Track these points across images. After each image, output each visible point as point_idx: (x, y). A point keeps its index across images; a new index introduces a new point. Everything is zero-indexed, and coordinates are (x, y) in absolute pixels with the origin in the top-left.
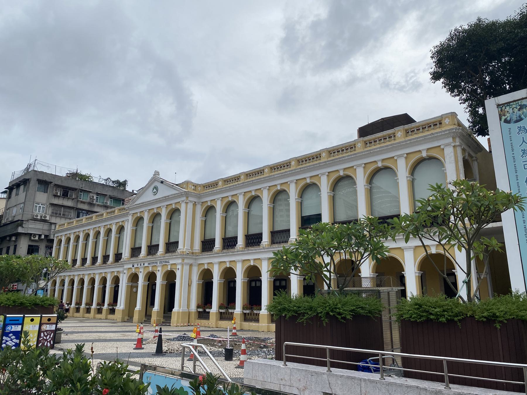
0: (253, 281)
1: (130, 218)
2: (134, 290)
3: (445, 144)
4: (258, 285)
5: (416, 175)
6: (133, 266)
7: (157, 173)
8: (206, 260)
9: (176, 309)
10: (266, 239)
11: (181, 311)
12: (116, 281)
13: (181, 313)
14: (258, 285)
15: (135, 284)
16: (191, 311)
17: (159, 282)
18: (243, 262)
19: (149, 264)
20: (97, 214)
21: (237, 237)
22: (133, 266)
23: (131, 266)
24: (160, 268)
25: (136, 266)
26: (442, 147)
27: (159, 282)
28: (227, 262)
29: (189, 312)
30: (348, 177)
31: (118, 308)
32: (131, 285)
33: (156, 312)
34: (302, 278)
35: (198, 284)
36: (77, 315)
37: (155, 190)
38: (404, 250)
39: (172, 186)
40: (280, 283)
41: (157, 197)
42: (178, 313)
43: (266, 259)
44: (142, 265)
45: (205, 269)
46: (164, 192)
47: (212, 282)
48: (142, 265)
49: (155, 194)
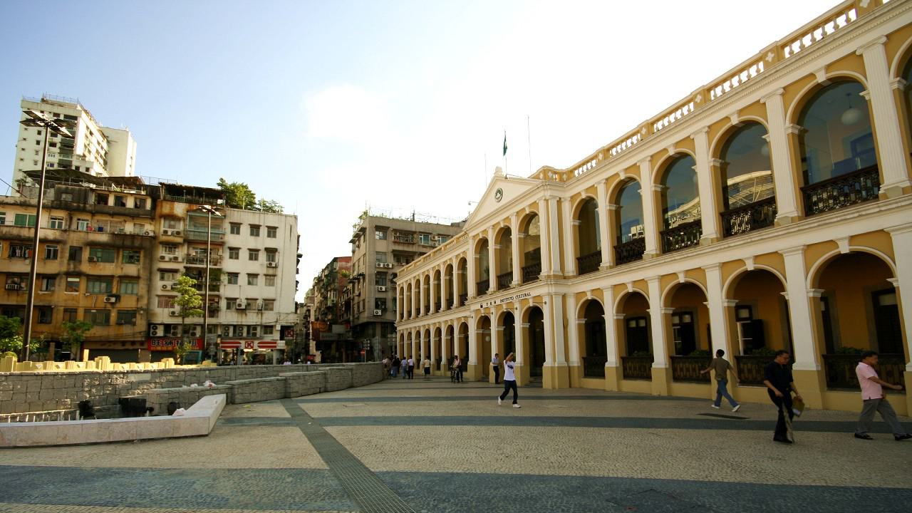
0: (632, 319)
1: (471, 241)
2: (487, 339)
3: (766, 95)
4: (642, 323)
5: (670, 181)
6: (482, 306)
7: (498, 169)
8: (588, 286)
9: (548, 363)
10: (652, 244)
11: (556, 365)
12: (464, 327)
13: (556, 369)
14: (642, 323)
15: (487, 332)
16: (571, 365)
17: (519, 325)
18: (721, 268)
19: (502, 301)
20: (425, 255)
21: (643, 240)
22: (482, 306)
23: (478, 307)
24: (517, 305)
25: (485, 306)
26: (691, 137)
27: (519, 325)
28: (628, 283)
29: (569, 367)
30: (631, 179)
31: (609, 366)
32: (481, 332)
33: (816, 373)
34: (734, 302)
35: (617, 320)
36: (438, 373)
37: (499, 195)
38: (891, 234)
39: (520, 181)
40: (637, 324)
41: (504, 201)
42: (552, 368)
43: (798, 250)
44: (493, 303)
45: (588, 300)
46: (511, 193)
47: (603, 321)
48: (493, 303)
49: (499, 200)
